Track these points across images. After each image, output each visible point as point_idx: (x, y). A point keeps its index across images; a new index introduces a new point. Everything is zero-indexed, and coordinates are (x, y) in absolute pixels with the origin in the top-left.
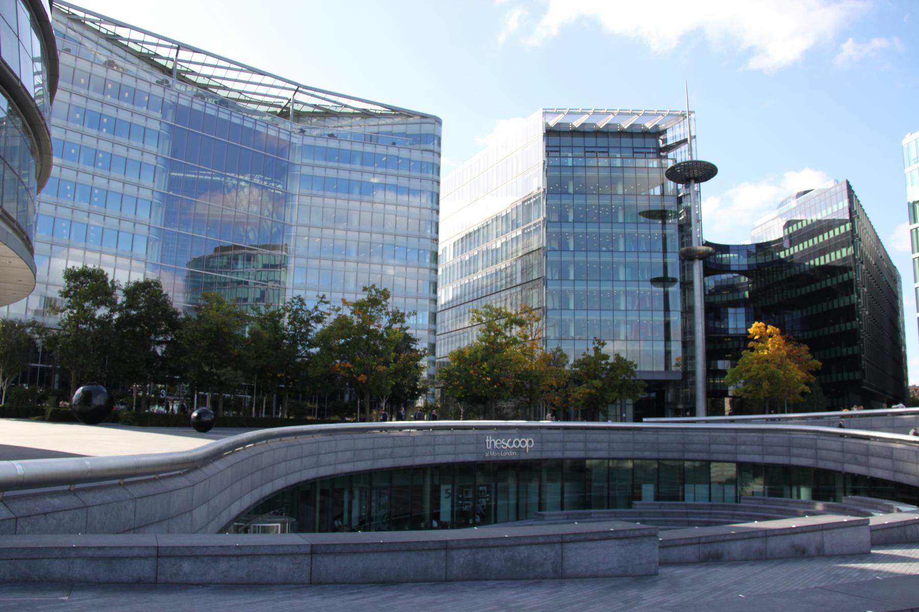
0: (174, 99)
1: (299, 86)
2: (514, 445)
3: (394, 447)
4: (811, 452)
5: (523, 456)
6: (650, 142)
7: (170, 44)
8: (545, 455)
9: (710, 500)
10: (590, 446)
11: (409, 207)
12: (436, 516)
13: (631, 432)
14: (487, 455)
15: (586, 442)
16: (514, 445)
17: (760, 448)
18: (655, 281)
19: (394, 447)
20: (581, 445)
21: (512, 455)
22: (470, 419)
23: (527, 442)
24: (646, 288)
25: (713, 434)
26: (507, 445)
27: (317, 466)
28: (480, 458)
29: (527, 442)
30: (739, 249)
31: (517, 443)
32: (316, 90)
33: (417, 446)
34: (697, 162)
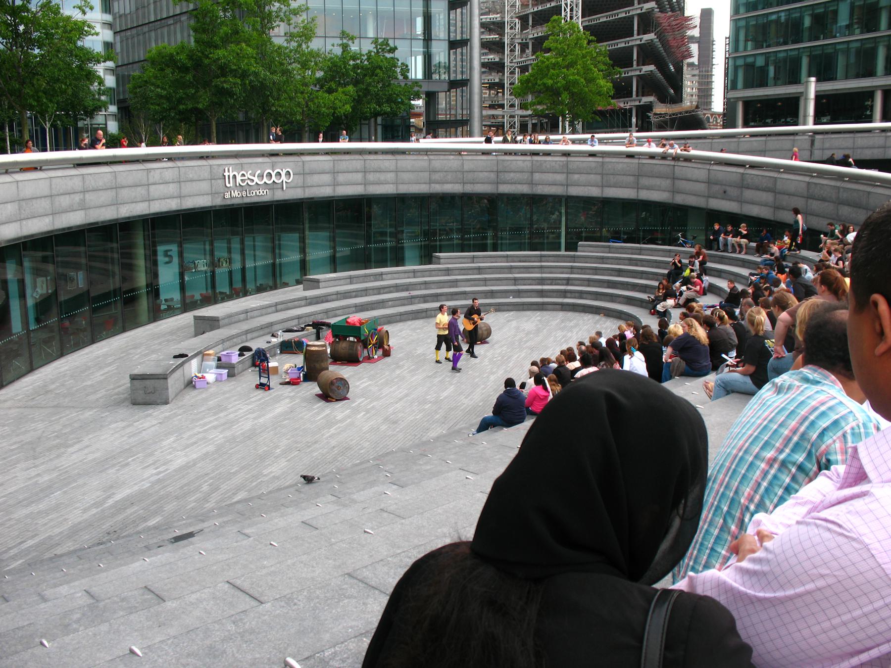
2: (265, 180)
3: (84, 192)
4: (666, 183)
5: (279, 196)
8: (309, 193)
10: (371, 177)
12: (154, 291)
14: (227, 196)
15: (334, 173)
16: (265, 180)
17: (599, 178)
19: (84, 192)
20: (359, 177)
21: (263, 195)
23: (283, 174)
26: (256, 179)
27: (116, 203)
28: (218, 202)
29: (283, 174)
31: (270, 175)
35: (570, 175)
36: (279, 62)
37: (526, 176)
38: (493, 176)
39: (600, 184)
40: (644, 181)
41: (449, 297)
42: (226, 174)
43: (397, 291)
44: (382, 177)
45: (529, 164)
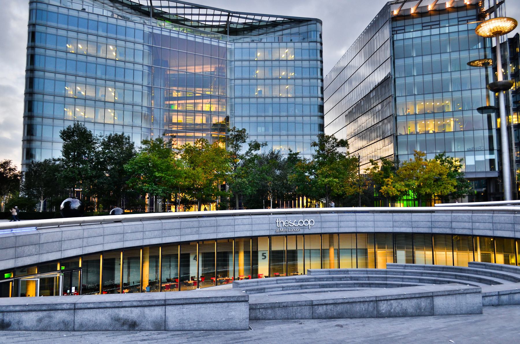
0: (150, 30)
1: (229, 12)
2: (299, 224)
7: (183, 5)
9: (433, 264)
13: (391, 214)
20: (353, 224)
24: (477, 114)
25: (454, 214)
26: (294, 224)
33: (219, 226)
35: (474, 224)
36: (94, 168)
37: (448, 224)
38: (429, 224)
39: (492, 229)
41: (513, 279)
42: (277, 221)
43: (351, 280)
44: (366, 224)
45: (450, 218)
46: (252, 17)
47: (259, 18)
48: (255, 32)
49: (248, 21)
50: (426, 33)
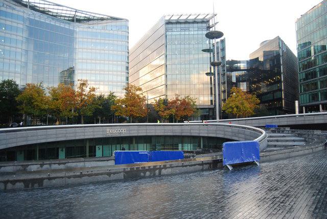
0: (28, 16)
1: (76, 10)
5: (122, 135)
6: (204, 25)
11: (4, 59)
18: (207, 74)
22: (103, 123)
28: (105, 136)
30: (243, 62)
32: (87, 12)
34: (217, 31)
40: (218, 132)
44: (151, 131)
46: (90, 14)
47: (94, 15)
48: (91, 22)
49: (87, 16)
50: (183, 33)
